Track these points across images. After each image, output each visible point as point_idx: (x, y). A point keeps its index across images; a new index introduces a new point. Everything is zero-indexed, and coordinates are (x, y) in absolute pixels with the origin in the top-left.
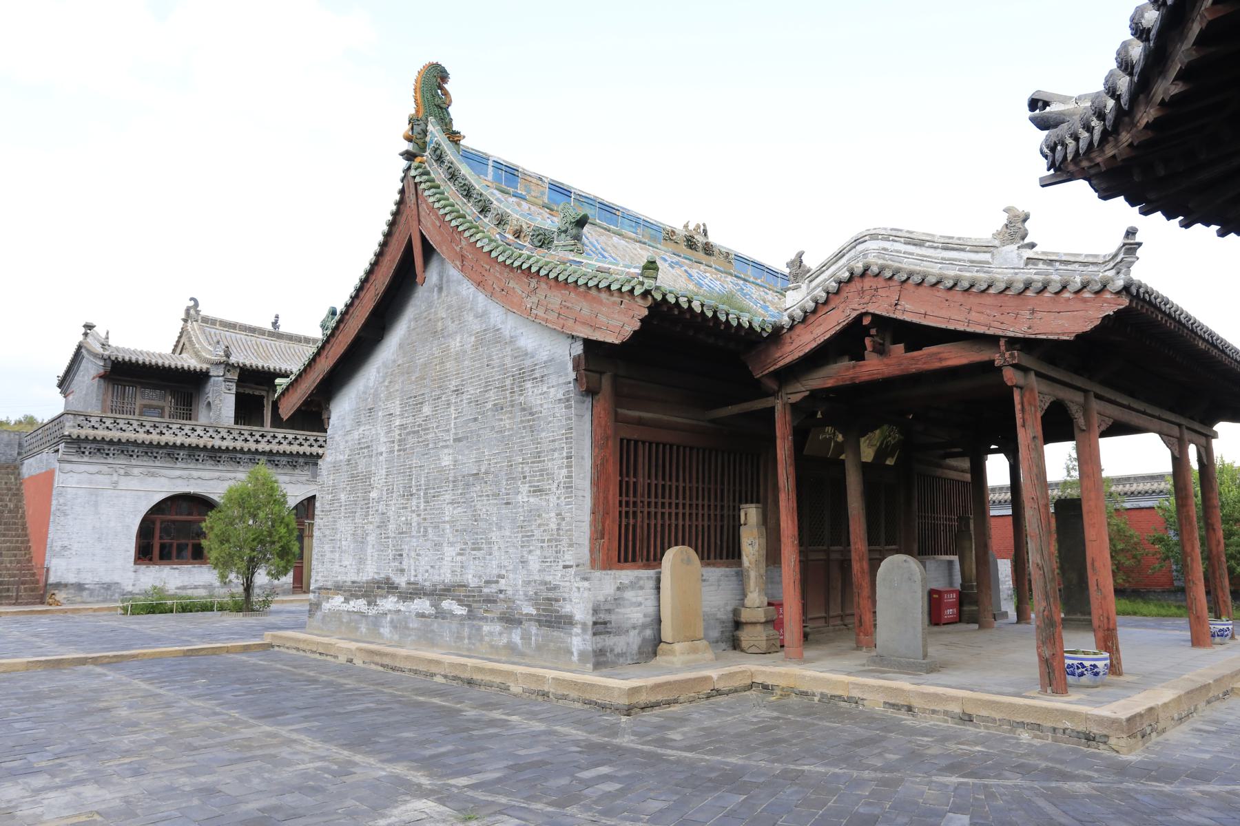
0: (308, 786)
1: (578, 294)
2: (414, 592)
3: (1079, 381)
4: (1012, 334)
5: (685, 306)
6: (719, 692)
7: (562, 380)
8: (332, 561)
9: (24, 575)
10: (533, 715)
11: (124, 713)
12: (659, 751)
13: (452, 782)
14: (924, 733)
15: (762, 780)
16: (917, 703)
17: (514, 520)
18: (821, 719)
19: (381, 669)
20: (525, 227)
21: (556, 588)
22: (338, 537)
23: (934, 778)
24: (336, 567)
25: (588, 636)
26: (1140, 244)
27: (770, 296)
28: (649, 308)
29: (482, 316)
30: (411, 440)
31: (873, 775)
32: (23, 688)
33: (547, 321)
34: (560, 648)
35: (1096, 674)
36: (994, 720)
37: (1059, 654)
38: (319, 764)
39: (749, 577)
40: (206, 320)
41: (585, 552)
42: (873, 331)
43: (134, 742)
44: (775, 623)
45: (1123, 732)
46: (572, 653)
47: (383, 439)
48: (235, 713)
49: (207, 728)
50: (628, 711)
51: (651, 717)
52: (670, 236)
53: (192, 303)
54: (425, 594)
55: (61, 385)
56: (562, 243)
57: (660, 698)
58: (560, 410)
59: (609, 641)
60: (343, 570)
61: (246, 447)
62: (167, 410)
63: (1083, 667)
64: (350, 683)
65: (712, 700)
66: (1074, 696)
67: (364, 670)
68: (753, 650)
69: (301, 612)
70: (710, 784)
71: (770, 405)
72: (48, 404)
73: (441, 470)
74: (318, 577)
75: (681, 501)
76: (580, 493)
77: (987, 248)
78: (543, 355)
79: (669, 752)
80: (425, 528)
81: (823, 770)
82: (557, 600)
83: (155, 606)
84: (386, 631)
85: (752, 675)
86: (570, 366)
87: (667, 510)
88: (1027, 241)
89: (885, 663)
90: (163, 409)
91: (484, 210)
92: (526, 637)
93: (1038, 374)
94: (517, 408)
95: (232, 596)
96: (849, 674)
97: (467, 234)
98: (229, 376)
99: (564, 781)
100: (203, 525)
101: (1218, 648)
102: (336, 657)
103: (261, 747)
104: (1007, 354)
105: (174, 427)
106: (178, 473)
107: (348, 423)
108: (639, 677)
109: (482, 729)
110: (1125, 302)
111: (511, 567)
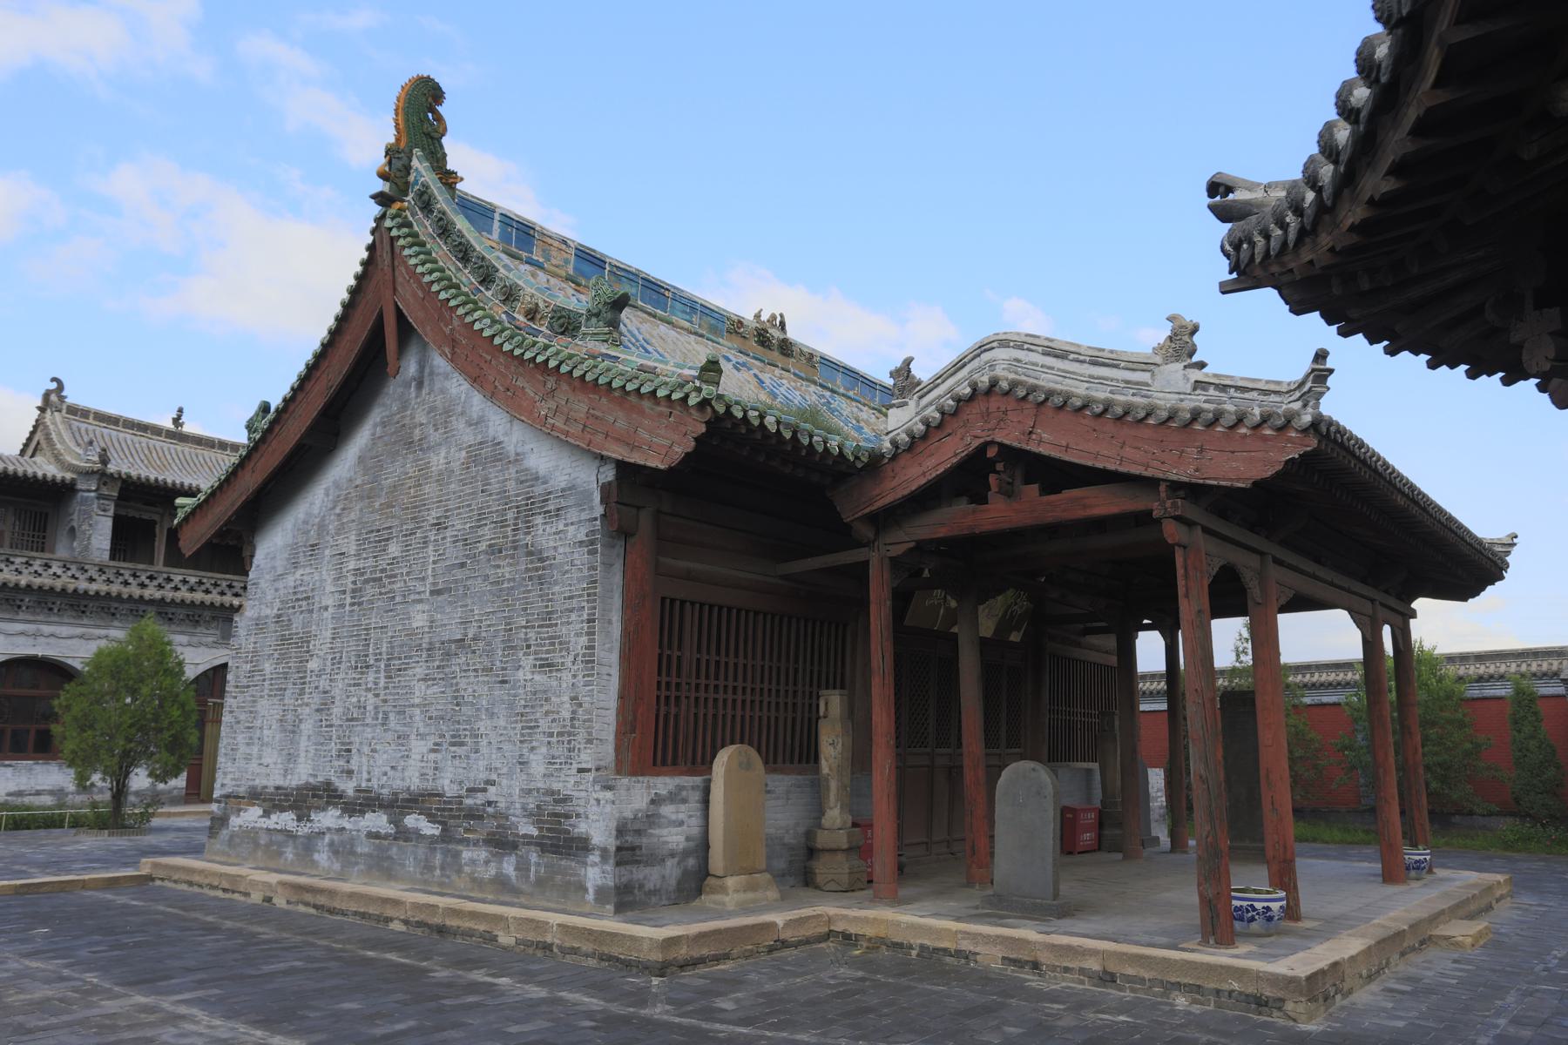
2: (365, 802)
4: (1175, 478)
5: (756, 423)
6: (785, 944)
7: (584, 516)
8: (248, 758)
10: (528, 977)
12: (705, 1025)
14: (1054, 997)
16: (1045, 958)
17: (511, 705)
19: (312, 911)
20: (541, 305)
21: (566, 799)
22: (258, 723)
24: (253, 766)
26: (1331, 371)
27: (866, 414)
29: (477, 423)
30: (370, 590)
33: (567, 434)
34: (569, 883)
35: (1270, 919)
36: (1143, 979)
39: (828, 788)
40: (73, 410)
42: (999, 467)
44: (861, 850)
45: (1301, 994)
46: (586, 890)
47: (330, 588)
48: (92, 978)
49: (48, 999)
50: (662, 969)
51: (689, 978)
52: (735, 327)
53: (54, 385)
54: (381, 806)
57: (705, 952)
58: (581, 556)
59: (639, 873)
60: (263, 770)
61: (126, 592)
63: (1254, 909)
64: (266, 932)
65: (776, 954)
66: (1243, 948)
67: (287, 913)
68: (833, 886)
69: (196, 829)
71: (863, 559)
73: (411, 634)
76: (604, 670)
77: (1146, 366)
78: (560, 481)
79: (718, 1026)
82: (567, 816)
84: (322, 857)
85: (830, 920)
86: (597, 497)
87: (721, 696)
88: (1195, 359)
89: (1004, 906)
92: (523, 867)
93: (1206, 530)
94: (521, 552)
95: (94, 805)
96: (958, 919)
97: (461, 311)
101: (1415, 884)
103: (130, 1027)
104: (1168, 503)
105: (18, 560)
107: (280, 564)
108: (677, 923)
109: (457, 996)
110: (1312, 443)
111: (505, 770)
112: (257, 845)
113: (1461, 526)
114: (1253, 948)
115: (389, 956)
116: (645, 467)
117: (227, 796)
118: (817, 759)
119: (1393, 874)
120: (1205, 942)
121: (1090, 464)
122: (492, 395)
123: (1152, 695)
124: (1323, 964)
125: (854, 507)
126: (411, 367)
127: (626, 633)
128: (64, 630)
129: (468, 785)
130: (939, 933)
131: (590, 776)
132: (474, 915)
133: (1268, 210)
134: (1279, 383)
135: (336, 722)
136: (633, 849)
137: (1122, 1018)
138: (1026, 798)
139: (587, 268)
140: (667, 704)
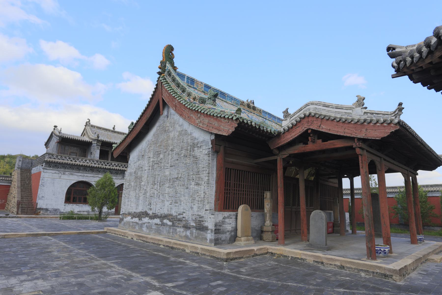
0: (116, 284)
1: (214, 119)
2: (154, 216)
3: (379, 154)
4: (359, 137)
5: (250, 124)
6: (256, 255)
7: (207, 148)
8: (128, 205)
9: (30, 205)
10: (193, 261)
11: (56, 253)
12: (238, 276)
13: (166, 285)
14: (328, 272)
15: (275, 288)
16: (325, 261)
17: (189, 194)
18: (292, 266)
19: (142, 242)
20: (197, 97)
21: (202, 217)
22: (130, 197)
23: (335, 289)
24: (129, 207)
25: (213, 234)
26: (403, 108)
27: (274, 124)
28: (238, 124)
29: (181, 126)
30: (156, 166)
31: (313, 287)
32: (24, 243)
33: (203, 127)
34: (203, 238)
35: (385, 253)
36: (352, 268)
37: (374, 246)
38: (120, 276)
40: (92, 126)
41: (213, 205)
42: (311, 135)
43: (57, 264)
44: (275, 231)
45: (398, 274)
46: (207, 240)
48: (92, 255)
49: (83, 260)
50: (226, 260)
51: (234, 263)
52: (242, 103)
54: (158, 217)
55: (45, 145)
56: (209, 102)
57: (237, 256)
58: (206, 157)
59: (220, 236)
60: (131, 208)
61: (102, 166)
62: (78, 154)
63: (381, 250)
64: (132, 246)
65: (255, 257)
66: (379, 261)
67: (137, 242)
68: (267, 240)
69: (117, 221)
70: (257, 289)
72: (41, 151)
73: (165, 176)
74: (123, 210)
75: (238, 189)
76: (212, 185)
77: (351, 108)
78: (201, 139)
79: (241, 276)
80: (159, 195)
81: (295, 285)
82: (203, 221)
83: (70, 217)
84: (144, 229)
85: (267, 249)
86: (210, 143)
87: (240, 192)
88: (364, 106)
89: (312, 247)
90: (77, 153)
91: (184, 91)
92: (192, 233)
93: (367, 151)
94: (191, 157)
95: (95, 215)
96: (301, 250)
97: (177, 99)
98: (98, 144)
99: (206, 286)
100: (88, 191)
101: (420, 244)
102: (128, 237)
103: (100, 268)
105: (80, 159)
106: (80, 174)
107: (136, 160)
108: (230, 249)
109: (176, 265)
110: (398, 127)
111: (187, 210)
112: (130, 225)
113: (433, 151)
114: (382, 261)
115: (160, 254)
116: (222, 135)
117: (123, 214)
118: (263, 208)
119: (414, 241)
120: (368, 258)
121: (336, 134)
122: (185, 119)
123: (347, 194)
124: (402, 266)
125: (274, 145)
126: (165, 113)
127: (217, 176)
128: (89, 175)
129: (179, 213)
130: (296, 253)
131: (208, 212)
132: (180, 245)
133: (407, 54)
134: (388, 112)
135: (148, 197)
136: (219, 230)
137: (348, 278)
138: (318, 219)
139: (207, 89)
140: (227, 194)
